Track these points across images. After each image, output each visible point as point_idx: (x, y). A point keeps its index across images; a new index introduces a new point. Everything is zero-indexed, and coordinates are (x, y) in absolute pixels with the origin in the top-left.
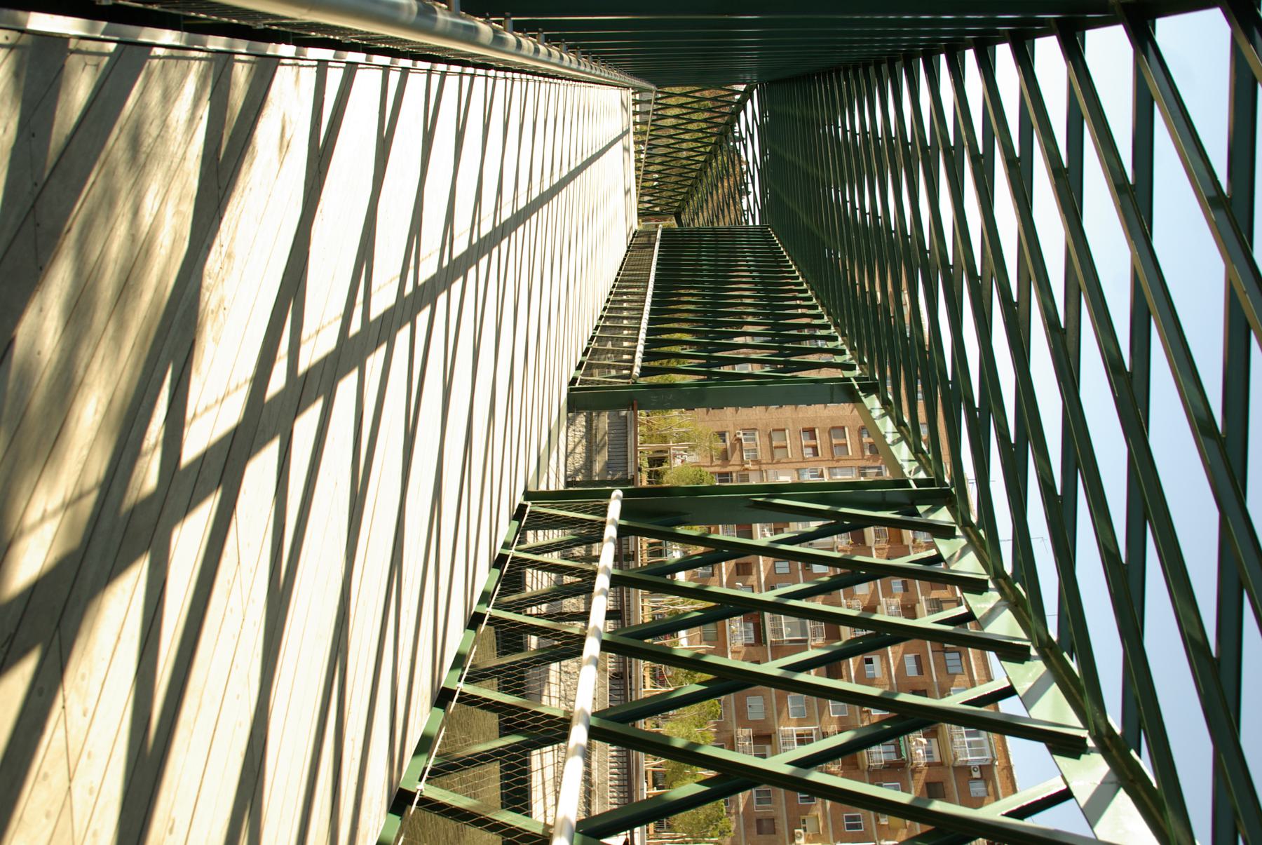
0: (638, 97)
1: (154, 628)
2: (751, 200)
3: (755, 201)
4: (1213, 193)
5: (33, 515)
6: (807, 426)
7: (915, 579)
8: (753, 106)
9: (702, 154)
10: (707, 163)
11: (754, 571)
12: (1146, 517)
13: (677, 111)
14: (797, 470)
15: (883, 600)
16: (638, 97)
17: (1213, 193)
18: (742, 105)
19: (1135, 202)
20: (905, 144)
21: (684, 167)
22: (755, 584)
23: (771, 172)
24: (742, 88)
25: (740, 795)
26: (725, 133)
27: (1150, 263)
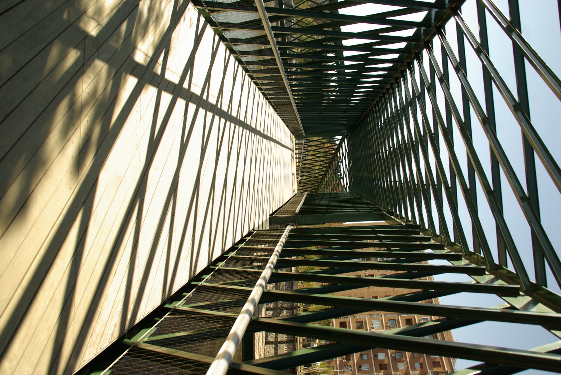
0: (297, 141)
1: (82, 240)
2: (345, 182)
3: (346, 167)
4: (522, 195)
5: (91, 5)
6: (374, 295)
7: (423, 352)
8: (345, 145)
9: (325, 167)
10: (327, 172)
11: (351, 359)
12: (506, 248)
13: (314, 148)
14: (370, 315)
15: (411, 372)
16: (297, 141)
17: (522, 195)
18: (340, 145)
19: (495, 199)
20: (405, 146)
21: (315, 177)
22: (352, 364)
23: (352, 171)
24: (340, 137)
25: (354, 354)
26: (333, 161)
27: (496, 143)
